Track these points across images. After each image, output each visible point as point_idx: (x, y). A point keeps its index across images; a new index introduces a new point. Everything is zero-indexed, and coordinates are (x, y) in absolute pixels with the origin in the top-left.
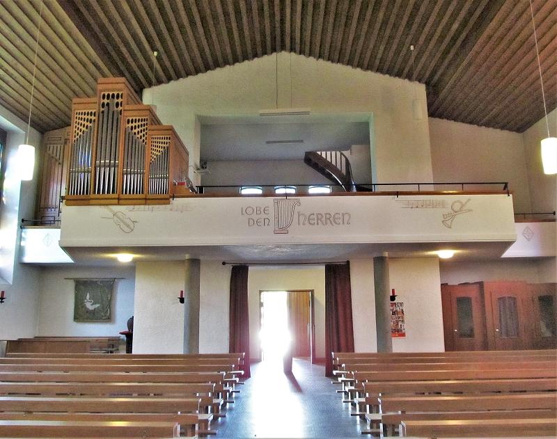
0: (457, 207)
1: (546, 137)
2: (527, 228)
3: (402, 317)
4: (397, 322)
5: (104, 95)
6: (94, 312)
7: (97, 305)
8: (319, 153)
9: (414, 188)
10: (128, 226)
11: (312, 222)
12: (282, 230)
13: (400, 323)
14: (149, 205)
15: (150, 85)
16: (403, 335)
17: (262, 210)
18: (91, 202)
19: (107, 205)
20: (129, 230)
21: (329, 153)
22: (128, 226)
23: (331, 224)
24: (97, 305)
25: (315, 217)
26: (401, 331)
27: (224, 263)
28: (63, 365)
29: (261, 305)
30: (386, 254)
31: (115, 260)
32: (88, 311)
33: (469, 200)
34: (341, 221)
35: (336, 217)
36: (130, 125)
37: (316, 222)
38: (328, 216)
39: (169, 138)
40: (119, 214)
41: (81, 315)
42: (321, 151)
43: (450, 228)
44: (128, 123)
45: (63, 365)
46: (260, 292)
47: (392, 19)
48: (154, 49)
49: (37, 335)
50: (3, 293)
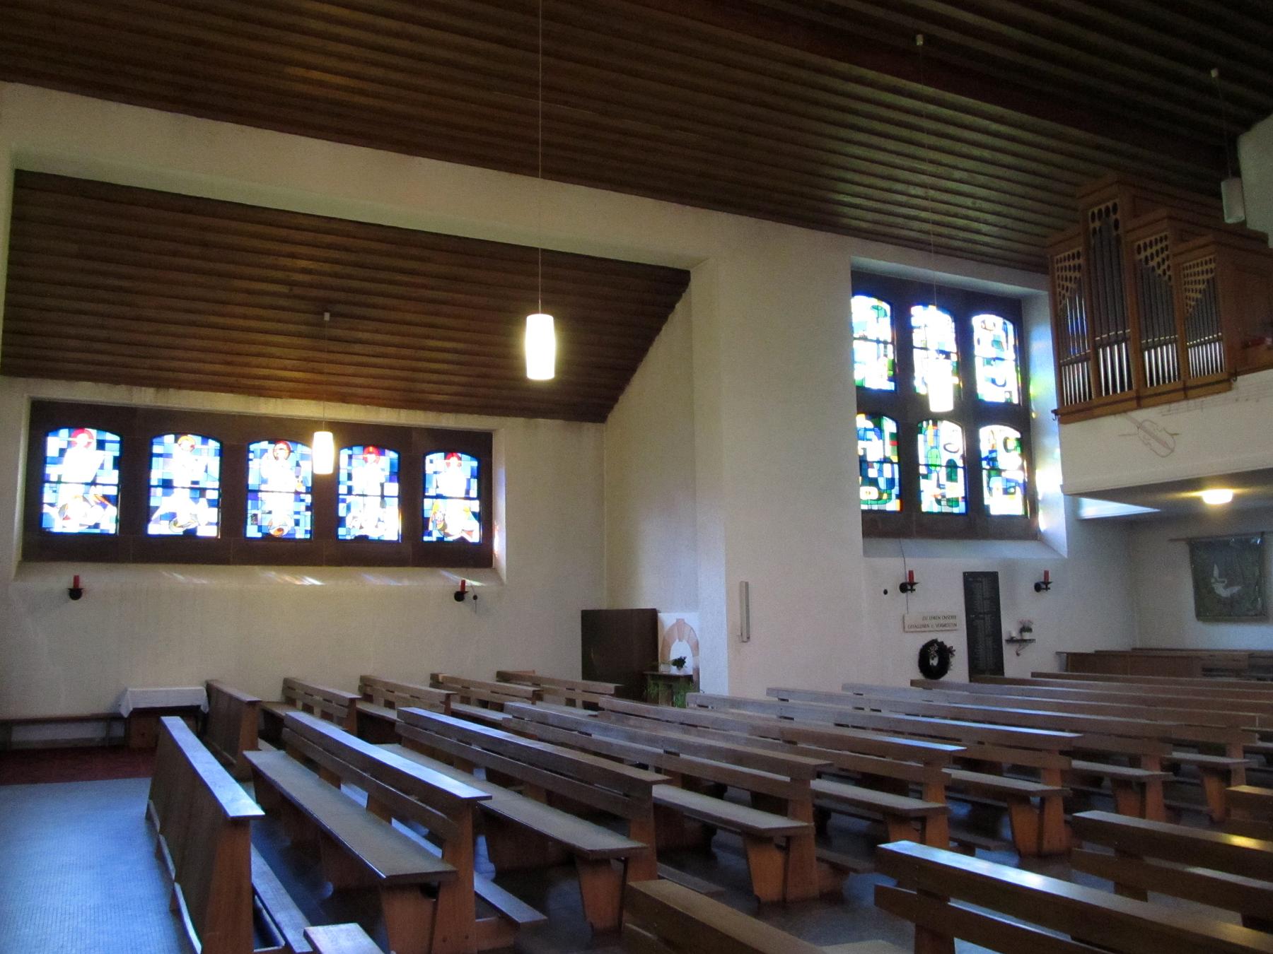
5: (1093, 214)
7: (1236, 589)
10: (1164, 444)
14: (1194, 398)
15: (1247, 125)
18: (1097, 411)
19: (1125, 411)
22: (1164, 444)
24: (1236, 589)
28: (1117, 719)
32: (1220, 600)
36: (1143, 255)
39: (1153, 269)
40: (1147, 424)
41: (1211, 609)
44: (1139, 253)
45: (706, 761)
47: (297, 291)
49: (1138, 645)
50: (1046, 573)
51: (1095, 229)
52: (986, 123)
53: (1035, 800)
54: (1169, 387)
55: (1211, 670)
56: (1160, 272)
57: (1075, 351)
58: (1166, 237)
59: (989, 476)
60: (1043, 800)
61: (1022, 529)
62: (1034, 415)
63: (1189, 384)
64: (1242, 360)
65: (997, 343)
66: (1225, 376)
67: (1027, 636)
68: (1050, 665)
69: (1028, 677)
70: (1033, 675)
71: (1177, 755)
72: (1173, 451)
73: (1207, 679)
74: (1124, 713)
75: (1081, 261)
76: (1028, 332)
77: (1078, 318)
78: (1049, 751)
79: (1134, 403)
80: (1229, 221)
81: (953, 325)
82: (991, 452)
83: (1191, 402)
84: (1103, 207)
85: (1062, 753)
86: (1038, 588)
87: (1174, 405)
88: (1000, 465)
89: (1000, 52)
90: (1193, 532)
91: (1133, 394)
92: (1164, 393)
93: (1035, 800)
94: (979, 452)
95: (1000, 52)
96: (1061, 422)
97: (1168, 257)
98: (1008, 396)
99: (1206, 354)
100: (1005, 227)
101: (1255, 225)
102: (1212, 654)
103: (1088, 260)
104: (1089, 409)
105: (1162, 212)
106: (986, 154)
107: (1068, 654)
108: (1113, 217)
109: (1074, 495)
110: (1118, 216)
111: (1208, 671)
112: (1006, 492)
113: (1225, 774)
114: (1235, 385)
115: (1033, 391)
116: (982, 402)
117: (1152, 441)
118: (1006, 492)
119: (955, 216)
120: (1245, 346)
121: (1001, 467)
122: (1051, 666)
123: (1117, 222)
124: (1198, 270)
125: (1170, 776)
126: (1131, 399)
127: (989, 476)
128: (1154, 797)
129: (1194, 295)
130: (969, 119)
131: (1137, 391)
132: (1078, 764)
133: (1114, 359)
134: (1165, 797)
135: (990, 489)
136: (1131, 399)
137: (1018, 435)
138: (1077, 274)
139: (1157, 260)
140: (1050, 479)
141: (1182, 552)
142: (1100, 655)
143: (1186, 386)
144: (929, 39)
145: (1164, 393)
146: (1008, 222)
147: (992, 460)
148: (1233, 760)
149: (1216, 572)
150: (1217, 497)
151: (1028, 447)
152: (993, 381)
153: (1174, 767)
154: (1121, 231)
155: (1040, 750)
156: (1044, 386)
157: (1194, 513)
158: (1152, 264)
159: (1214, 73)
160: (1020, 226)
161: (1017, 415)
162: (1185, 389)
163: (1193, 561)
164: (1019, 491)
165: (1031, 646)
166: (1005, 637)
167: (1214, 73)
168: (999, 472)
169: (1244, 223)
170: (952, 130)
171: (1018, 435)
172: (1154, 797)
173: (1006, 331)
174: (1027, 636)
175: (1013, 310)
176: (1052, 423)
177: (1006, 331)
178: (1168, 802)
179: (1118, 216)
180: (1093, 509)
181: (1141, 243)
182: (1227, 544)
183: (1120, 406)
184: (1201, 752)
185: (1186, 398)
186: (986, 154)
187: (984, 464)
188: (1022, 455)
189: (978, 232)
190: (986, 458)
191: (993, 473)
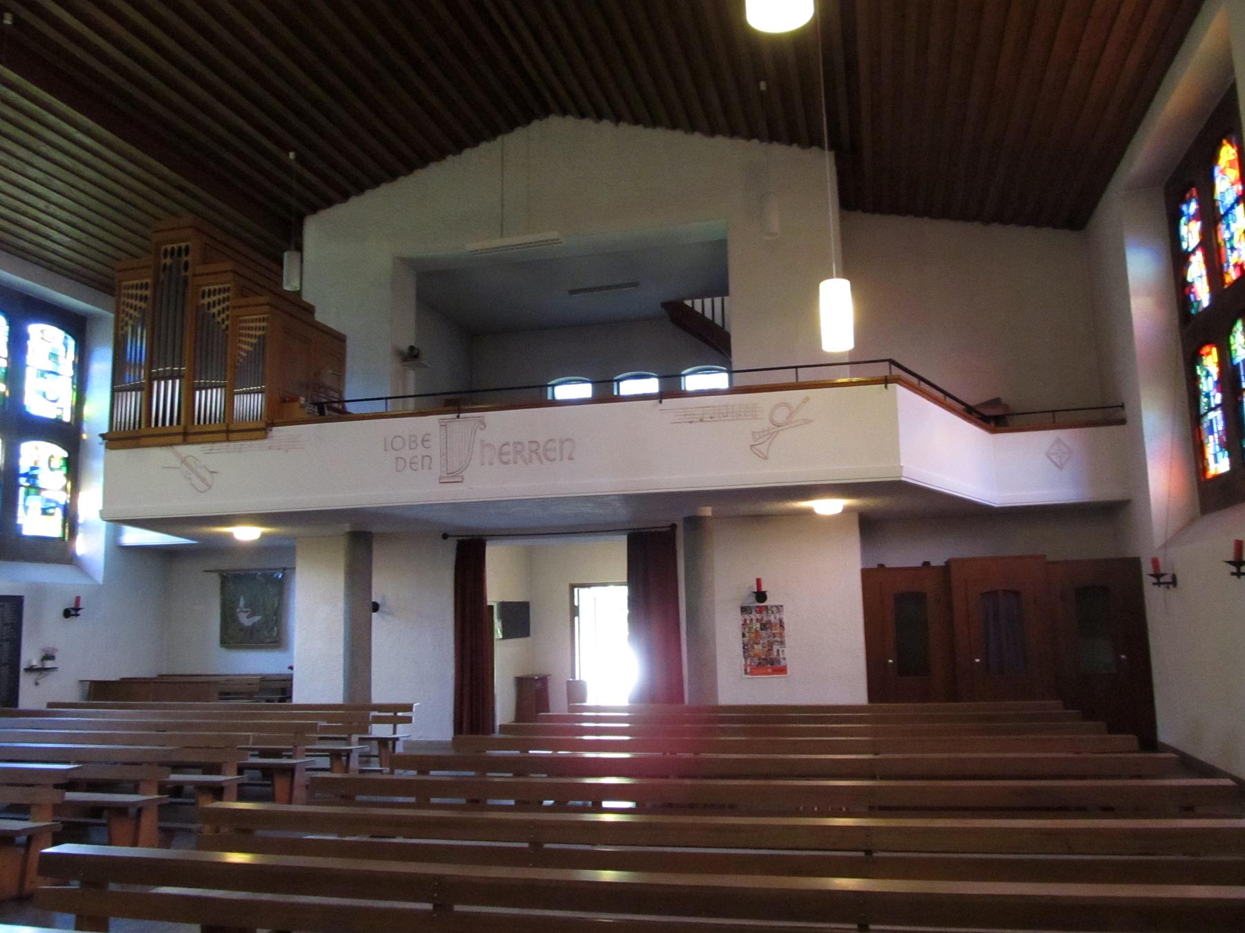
0: (781, 416)
1: (829, 276)
2: (1059, 440)
3: (781, 635)
4: (771, 645)
6: (252, 630)
7: (257, 618)
8: (688, 303)
9: (788, 377)
10: (203, 480)
11: (505, 458)
12: (453, 477)
13: (775, 647)
14: (193, 443)
15: (314, 210)
16: (783, 670)
17: (419, 441)
18: (144, 441)
19: (171, 445)
20: (203, 487)
21: (708, 301)
22: (203, 480)
23: (540, 459)
24: (257, 618)
25: (510, 448)
26: (779, 662)
27: (445, 536)
29: (574, 611)
30: (707, 511)
31: (229, 537)
32: (242, 629)
33: (807, 399)
34: (419, 465)
35: (548, 446)
36: (206, 300)
37: (511, 457)
38: (534, 446)
40: (189, 460)
42: (693, 298)
43: (766, 458)
44: (203, 297)
46: (573, 587)
48: (287, 149)
50: (78, 599)
51: (165, 266)
52: (73, 131)
53: (132, 811)
54: (215, 429)
55: (228, 694)
56: (219, 319)
57: (130, 378)
58: (229, 290)
59: (27, 494)
60: (30, 839)
61: (55, 552)
62: (84, 436)
63: (232, 427)
64: (279, 413)
65: (53, 356)
66: (262, 425)
67: (49, 664)
68: (72, 694)
69: (43, 707)
70: (50, 705)
71: (175, 777)
72: (210, 487)
73: (222, 703)
74: (132, 740)
75: (148, 293)
76: (90, 352)
77: (138, 346)
78: (45, 786)
79: (180, 438)
80: (286, 288)
81: (7, 328)
82: (33, 468)
83: (232, 444)
84: (176, 246)
85: (56, 786)
86: (67, 613)
87: (217, 445)
88: (41, 483)
89: (93, 62)
90: (226, 564)
91: (180, 429)
92: (205, 433)
93: (132, 811)
94: (17, 468)
95: (93, 62)
96: (108, 447)
97: (228, 308)
98: (59, 412)
99: (250, 403)
100: (78, 240)
101: (308, 297)
102: (230, 679)
103: (155, 292)
104: (138, 438)
105: (228, 266)
106: (67, 161)
107: (92, 682)
108: (184, 258)
109: (117, 522)
110: (189, 258)
111: (225, 695)
112: (45, 512)
113: (218, 792)
114: (270, 434)
115: (88, 411)
116: (28, 415)
117: (193, 476)
118: (45, 512)
119: (24, 214)
120: (284, 401)
121: (41, 486)
122: (73, 696)
123: (186, 264)
124: (254, 325)
125: (166, 799)
126: (177, 434)
127: (27, 494)
128: (149, 822)
129: (246, 347)
130: (51, 119)
131: (185, 428)
132: (70, 796)
133: (167, 393)
134: (160, 820)
135: (26, 508)
136: (177, 434)
137: (65, 454)
138: (143, 305)
139: (218, 308)
140: (91, 502)
141: (214, 581)
142: (125, 682)
143: (229, 429)
144: (17, 20)
145: (205, 433)
146: (83, 236)
147: (31, 477)
148: (227, 777)
149: (242, 603)
150: (247, 534)
151: (74, 469)
152: (44, 396)
153: (177, 790)
154: (189, 273)
155: (32, 785)
156: (97, 410)
157: (228, 548)
158: (214, 310)
159: (292, 155)
160: (91, 241)
161: (66, 434)
162: (228, 432)
163: (222, 593)
164: (59, 513)
165: (54, 673)
166: (24, 664)
167: (292, 155)
168: (39, 490)
169: (298, 294)
170: (34, 126)
171: (65, 454)
172: (149, 822)
173: (66, 345)
174: (49, 664)
175: (76, 325)
176: (99, 447)
177: (66, 345)
178: (162, 824)
179: (189, 258)
180: (134, 536)
181: (206, 289)
182: (254, 577)
183: (167, 439)
184: (204, 773)
185: (228, 440)
186: (67, 161)
187: (22, 481)
188: (68, 476)
189: (47, 237)
190: (26, 475)
191: (33, 491)
